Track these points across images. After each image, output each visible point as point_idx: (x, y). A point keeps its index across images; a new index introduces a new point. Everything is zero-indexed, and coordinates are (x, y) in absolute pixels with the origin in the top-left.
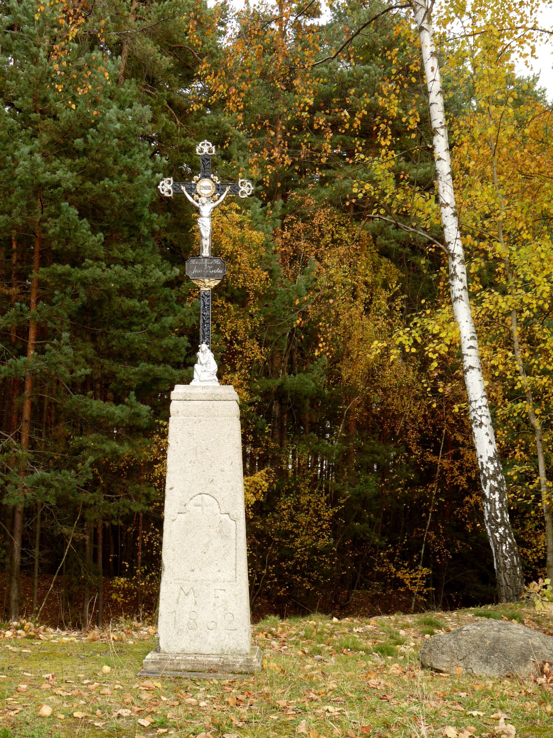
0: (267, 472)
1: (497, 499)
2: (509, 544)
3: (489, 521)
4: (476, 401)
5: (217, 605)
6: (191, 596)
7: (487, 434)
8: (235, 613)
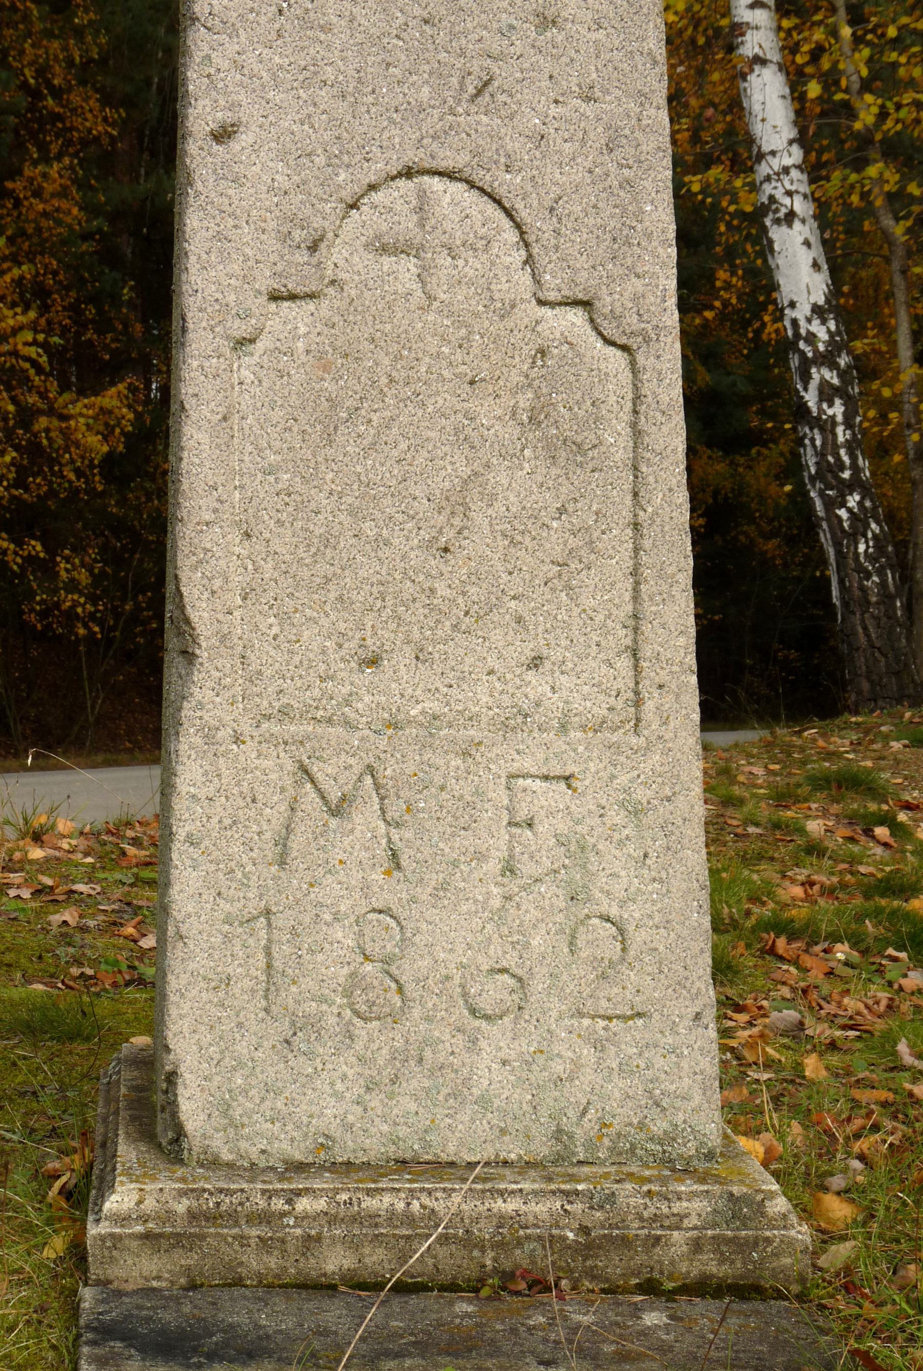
0: (130, 388)
1: (840, 418)
2: (875, 537)
3: (820, 475)
4: (773, 153)
5: (527, 868)
6: (366, 818)
7: (807, 243)
8: (634, 913)
